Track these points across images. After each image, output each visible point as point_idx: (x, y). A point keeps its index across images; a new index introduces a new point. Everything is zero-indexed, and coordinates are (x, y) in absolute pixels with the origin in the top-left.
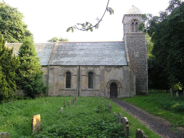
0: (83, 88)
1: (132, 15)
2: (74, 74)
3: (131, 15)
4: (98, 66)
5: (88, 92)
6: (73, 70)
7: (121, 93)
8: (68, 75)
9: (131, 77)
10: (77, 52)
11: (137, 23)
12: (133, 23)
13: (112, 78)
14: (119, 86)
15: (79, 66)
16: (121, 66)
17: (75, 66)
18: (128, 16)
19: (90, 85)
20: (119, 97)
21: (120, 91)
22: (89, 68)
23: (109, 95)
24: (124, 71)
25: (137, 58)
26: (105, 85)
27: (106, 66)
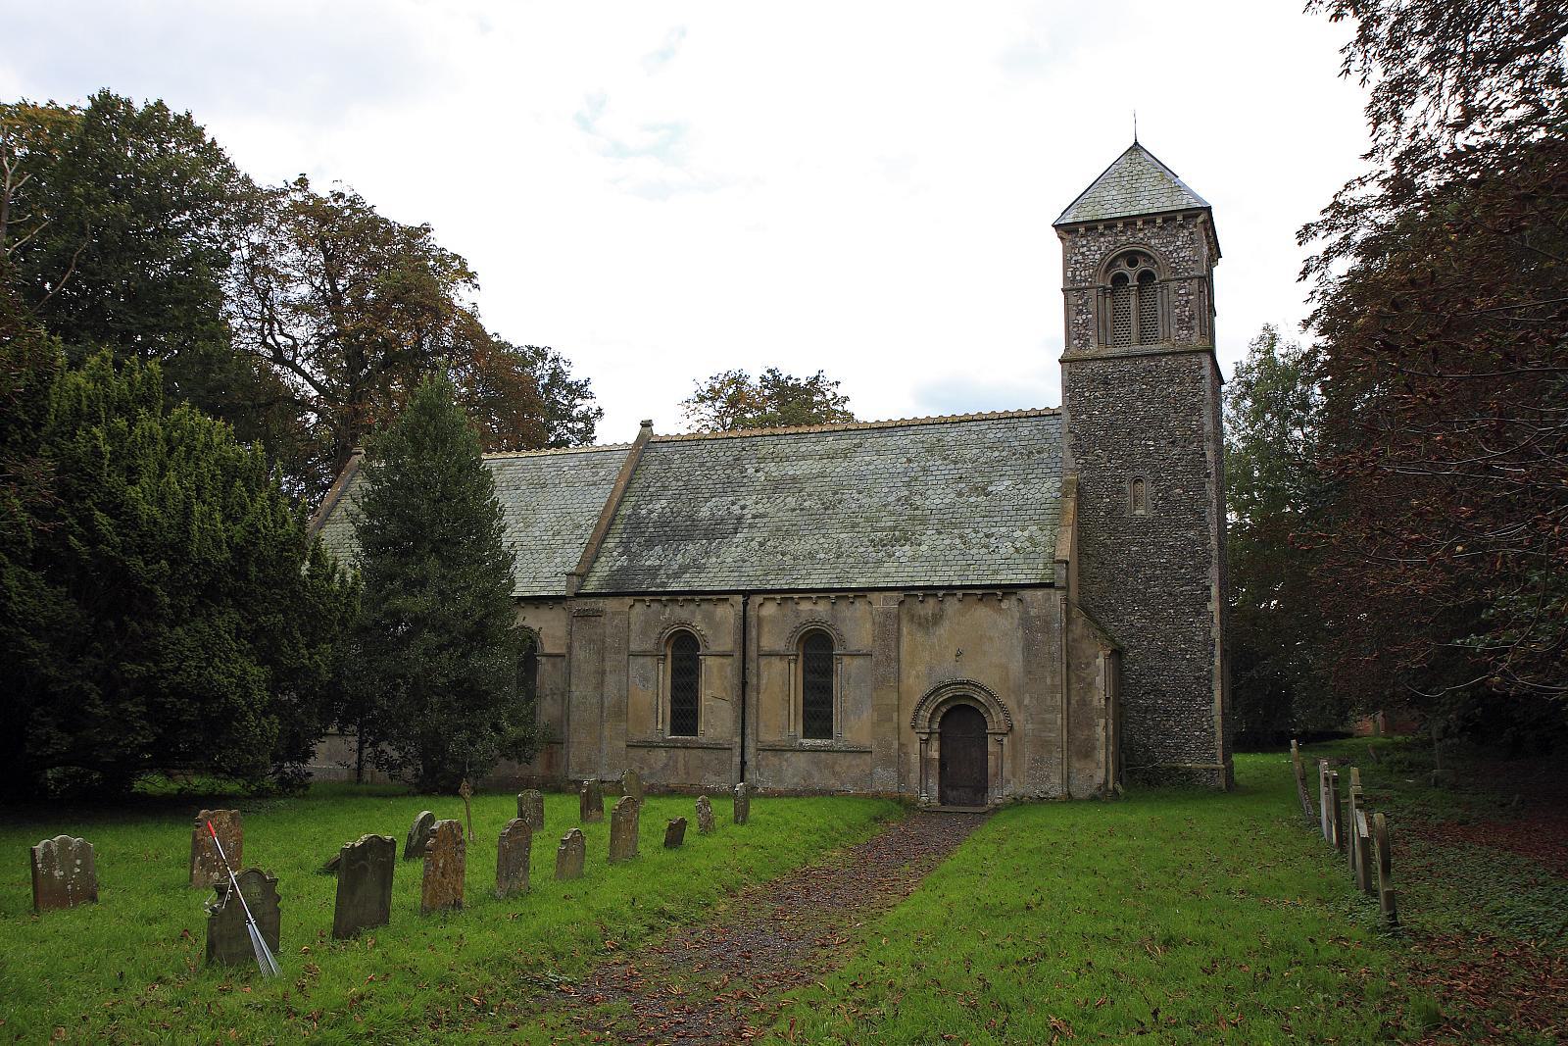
0: (769, 737)
1: (1110, 224)
2: (714, 648)
3: (1101, 228)
4: (862, 592)
5: (801, 761)
6: (709, 618)
7: (1006, 773)
8: (685, 650)
9: (1073, 665)
10: (751, 504)
11: (1146, 278)
12: (1120, 280)
13: (948, 670)
14: (995, 721)
15: (747, 594)
16: (1010, 589)
17: (721, 596)
18: (1082, 230)
19: (818, 716)
20: (995, 796)
21: (1000, 757)
22: (805, 606)
23: (934, 784)
24: (1026, 623)
25: (1145, 527)
26: (906, 720)
27: (908, 590)
